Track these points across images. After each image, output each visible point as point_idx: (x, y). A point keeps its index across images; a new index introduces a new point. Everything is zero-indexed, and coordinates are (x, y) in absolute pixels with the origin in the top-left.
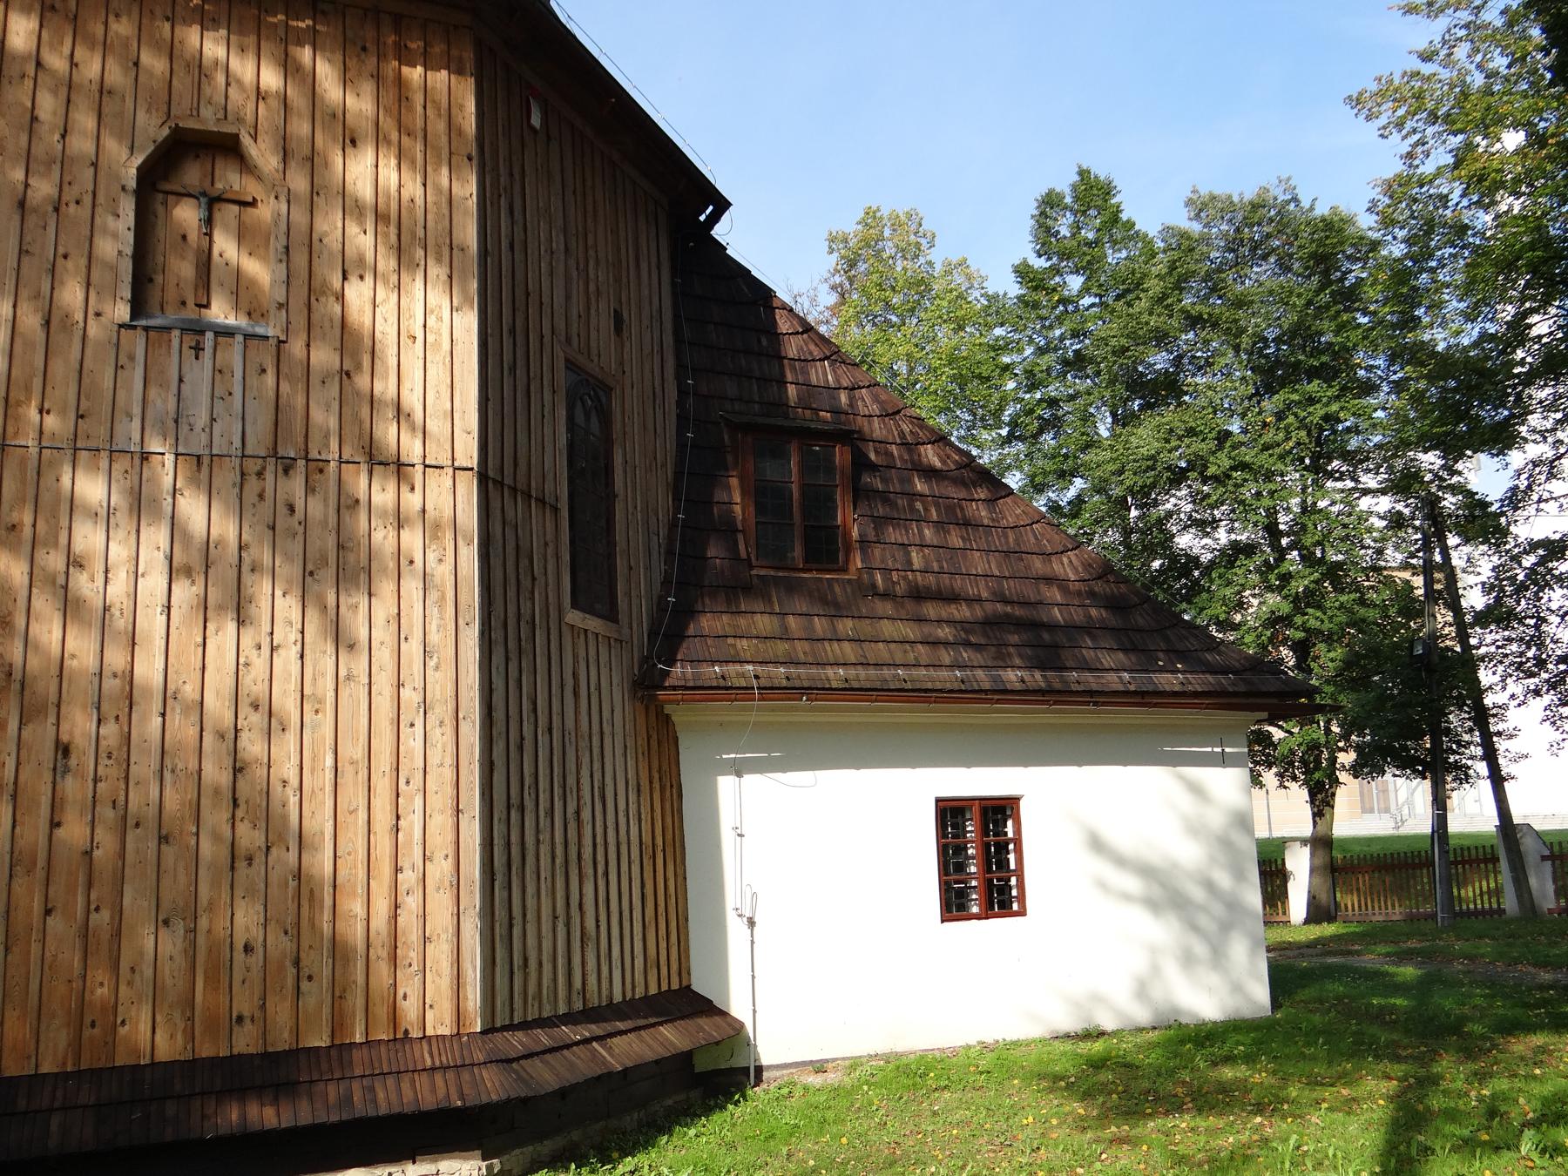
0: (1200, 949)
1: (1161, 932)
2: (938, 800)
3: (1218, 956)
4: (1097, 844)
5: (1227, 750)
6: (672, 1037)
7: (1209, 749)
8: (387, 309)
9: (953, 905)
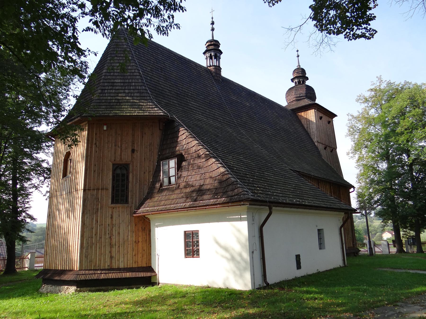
0: (238, 272)
1: (230, 266)
2: (185, 232)
3: (241, 276)
4: (217, 243)
5: (242, 216)
6: (149, 274)
7: (237, 217)
8: (184, 137)
9: (320, 249)
